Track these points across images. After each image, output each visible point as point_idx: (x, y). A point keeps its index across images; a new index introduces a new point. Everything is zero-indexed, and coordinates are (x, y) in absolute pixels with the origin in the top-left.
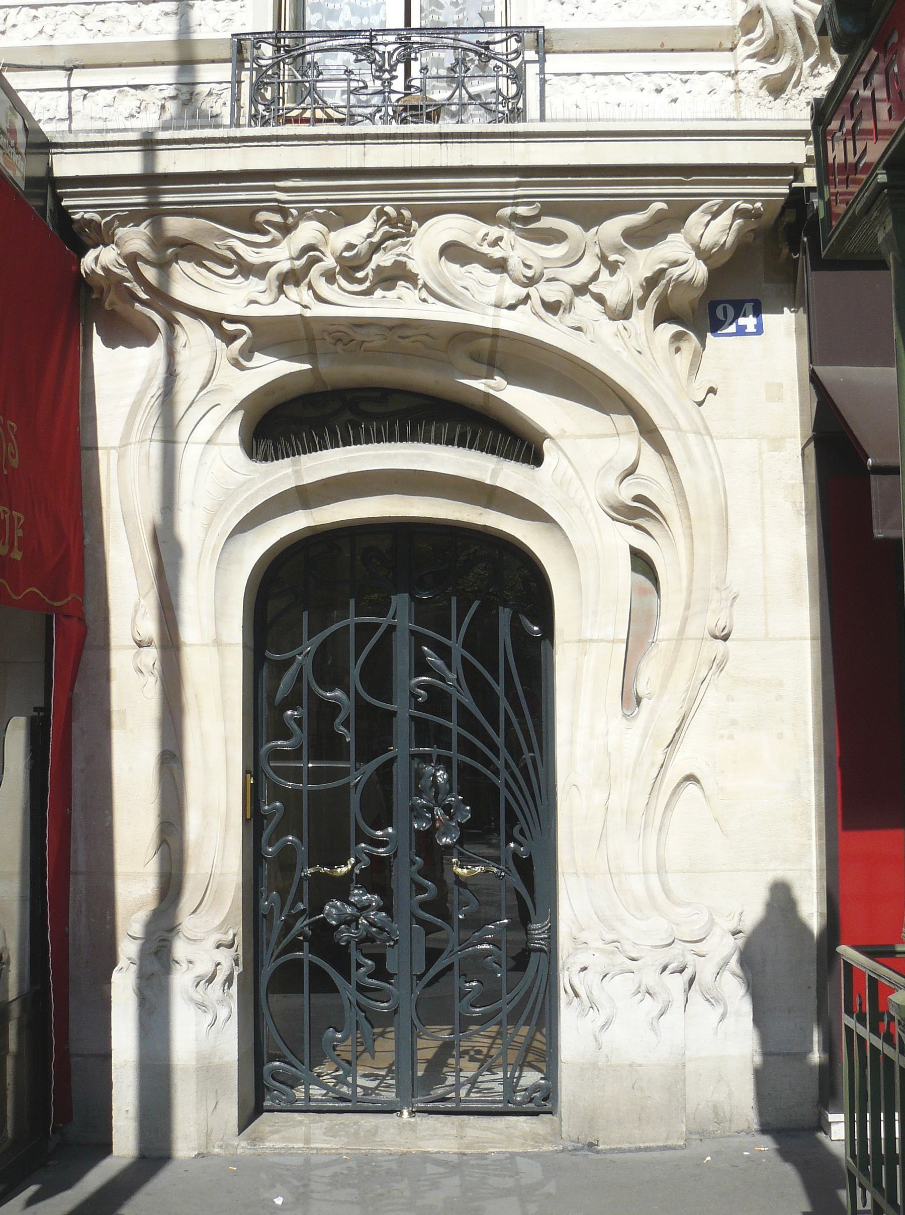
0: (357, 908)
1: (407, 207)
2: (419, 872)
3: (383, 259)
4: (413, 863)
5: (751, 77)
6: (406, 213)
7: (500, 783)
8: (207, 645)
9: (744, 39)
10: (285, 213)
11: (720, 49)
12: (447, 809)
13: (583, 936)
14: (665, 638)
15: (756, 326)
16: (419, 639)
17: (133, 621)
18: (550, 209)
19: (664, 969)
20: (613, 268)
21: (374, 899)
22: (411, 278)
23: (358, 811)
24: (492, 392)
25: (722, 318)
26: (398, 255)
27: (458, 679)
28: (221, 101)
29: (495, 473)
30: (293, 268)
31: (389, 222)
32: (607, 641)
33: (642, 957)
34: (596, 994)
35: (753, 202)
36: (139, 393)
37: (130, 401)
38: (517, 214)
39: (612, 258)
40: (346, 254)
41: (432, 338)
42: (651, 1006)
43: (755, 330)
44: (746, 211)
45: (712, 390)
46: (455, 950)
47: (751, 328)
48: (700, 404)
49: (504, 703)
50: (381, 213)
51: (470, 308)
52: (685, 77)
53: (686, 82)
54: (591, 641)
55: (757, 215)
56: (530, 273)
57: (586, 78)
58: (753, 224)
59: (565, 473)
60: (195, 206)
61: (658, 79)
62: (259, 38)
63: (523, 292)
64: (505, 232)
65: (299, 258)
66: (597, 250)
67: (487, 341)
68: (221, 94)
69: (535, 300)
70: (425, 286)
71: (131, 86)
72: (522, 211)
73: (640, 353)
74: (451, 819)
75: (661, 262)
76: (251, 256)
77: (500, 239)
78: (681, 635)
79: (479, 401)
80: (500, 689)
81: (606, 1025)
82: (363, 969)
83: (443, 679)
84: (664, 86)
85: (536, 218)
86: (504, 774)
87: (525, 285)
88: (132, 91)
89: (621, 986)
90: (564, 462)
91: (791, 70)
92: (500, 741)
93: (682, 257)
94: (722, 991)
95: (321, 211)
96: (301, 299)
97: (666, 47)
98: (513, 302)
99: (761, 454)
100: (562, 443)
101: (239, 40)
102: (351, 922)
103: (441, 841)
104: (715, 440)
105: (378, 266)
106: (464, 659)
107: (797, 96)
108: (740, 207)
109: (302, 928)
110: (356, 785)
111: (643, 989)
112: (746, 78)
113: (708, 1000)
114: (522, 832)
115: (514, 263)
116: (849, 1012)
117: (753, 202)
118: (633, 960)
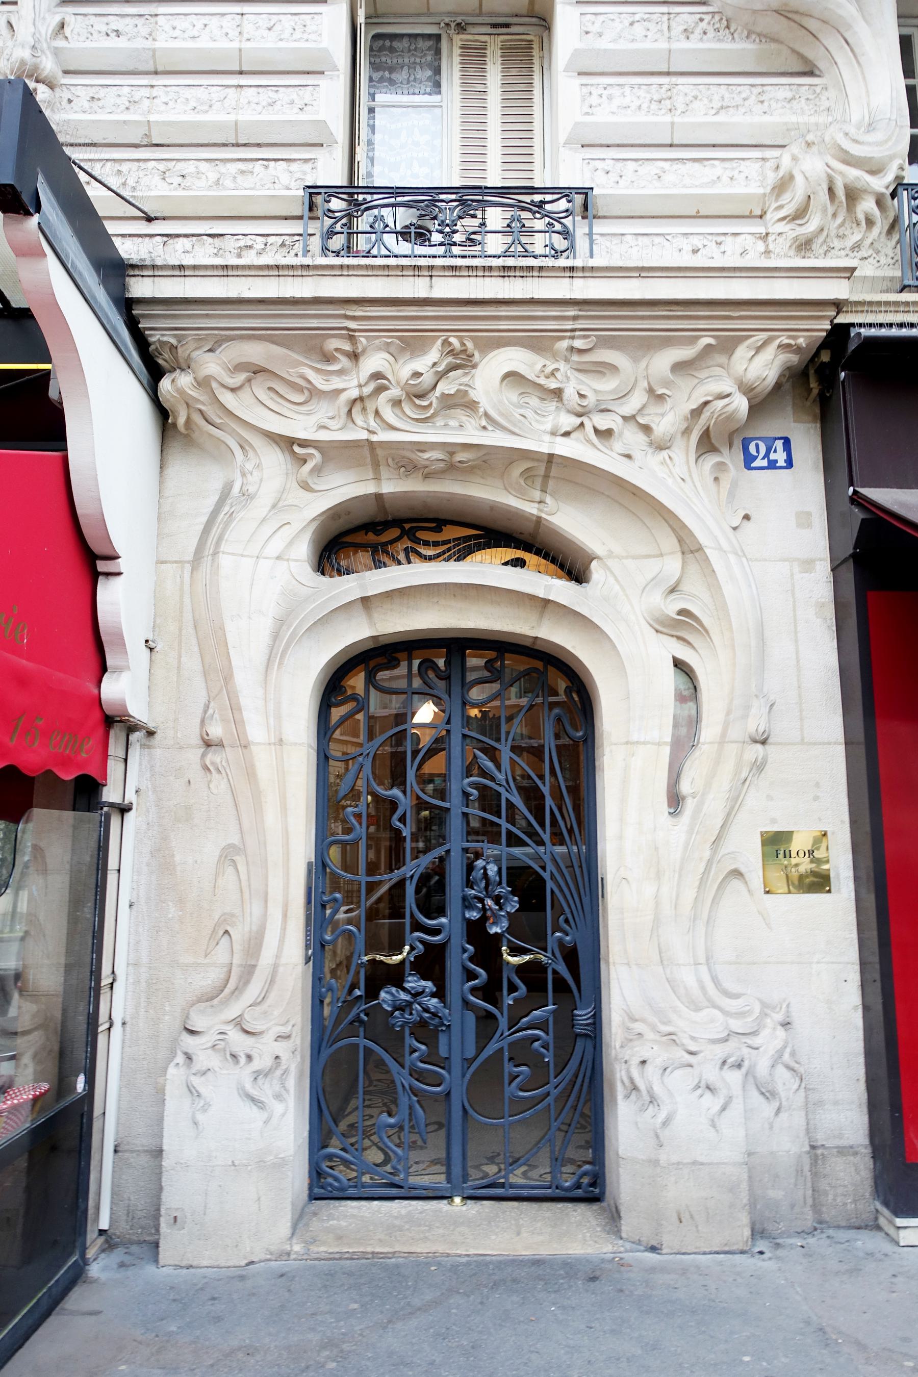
0: (411, 994)
2: (471, 959)
3: (444, 387)
4: (465, 950)
5: (780, 240)
6: (470, 345)
7: (546, 876)
9: (774, 205)
10: (352, 339)
11: (750, 216)
12: (497, 899)
13: (639, 1027)
14: (708, 741)
17: (203, 722)
19: (724, 1062)
21: (429, 985)
22: (471, 406)
23: (413, 901)
24: (544, 516)
25: (755, 453)
26: (460, 385)
28: (293, 253)
31: (452, 352)
32: (653, 744)
33: (701, 1052)
34: (657, 1089)
36: (212, 512)
37: (204, 519)
39: (660, 392)
40: (412, 382)
42: (711, 1103)
44: (789, 345)
45: (747, 517)
47: (781, 463)
49: (549, 802)
50: (446, 342)
51: (527, 435)
52: (720, 239)
53: (720, 244)
54: (637, 742)
55: (798, 350)
57: (629, 238)
62: (332, 191)
63: (578, 421)
64: (562, 365)
66: (646, 385)
70: (486, 414)
71: (209, 235)
72: (579, 344)
73: (683, 480)
74: (501, 909)
75: (706, 395)
76: (318, 382)
77: (557, 370)
78: (723, 740)
79: (529, 527)
80: (546, 790)
81: (665, 1123)
82: (416, 1054)
83: (493, 779)
84: (701, 246)
87: (580, 415)
88: (210, 240)
89: (680, 1080)
90: (611, 580)
93: (728, 390)
96: (369, 425)
97: (701, 214)
98: (568, 429)
99: (792, 575)
100: (610, 562)
101: (311, 194)
102: (402, 1007)
105: (443, 394)
109: (358, 1014)
110: (412, 877)
111: (703, 1084)
113: (763, 1093)
114: (567, 921)
115: (570, 393)
116: (698, 1009)
118: (691, 1053)
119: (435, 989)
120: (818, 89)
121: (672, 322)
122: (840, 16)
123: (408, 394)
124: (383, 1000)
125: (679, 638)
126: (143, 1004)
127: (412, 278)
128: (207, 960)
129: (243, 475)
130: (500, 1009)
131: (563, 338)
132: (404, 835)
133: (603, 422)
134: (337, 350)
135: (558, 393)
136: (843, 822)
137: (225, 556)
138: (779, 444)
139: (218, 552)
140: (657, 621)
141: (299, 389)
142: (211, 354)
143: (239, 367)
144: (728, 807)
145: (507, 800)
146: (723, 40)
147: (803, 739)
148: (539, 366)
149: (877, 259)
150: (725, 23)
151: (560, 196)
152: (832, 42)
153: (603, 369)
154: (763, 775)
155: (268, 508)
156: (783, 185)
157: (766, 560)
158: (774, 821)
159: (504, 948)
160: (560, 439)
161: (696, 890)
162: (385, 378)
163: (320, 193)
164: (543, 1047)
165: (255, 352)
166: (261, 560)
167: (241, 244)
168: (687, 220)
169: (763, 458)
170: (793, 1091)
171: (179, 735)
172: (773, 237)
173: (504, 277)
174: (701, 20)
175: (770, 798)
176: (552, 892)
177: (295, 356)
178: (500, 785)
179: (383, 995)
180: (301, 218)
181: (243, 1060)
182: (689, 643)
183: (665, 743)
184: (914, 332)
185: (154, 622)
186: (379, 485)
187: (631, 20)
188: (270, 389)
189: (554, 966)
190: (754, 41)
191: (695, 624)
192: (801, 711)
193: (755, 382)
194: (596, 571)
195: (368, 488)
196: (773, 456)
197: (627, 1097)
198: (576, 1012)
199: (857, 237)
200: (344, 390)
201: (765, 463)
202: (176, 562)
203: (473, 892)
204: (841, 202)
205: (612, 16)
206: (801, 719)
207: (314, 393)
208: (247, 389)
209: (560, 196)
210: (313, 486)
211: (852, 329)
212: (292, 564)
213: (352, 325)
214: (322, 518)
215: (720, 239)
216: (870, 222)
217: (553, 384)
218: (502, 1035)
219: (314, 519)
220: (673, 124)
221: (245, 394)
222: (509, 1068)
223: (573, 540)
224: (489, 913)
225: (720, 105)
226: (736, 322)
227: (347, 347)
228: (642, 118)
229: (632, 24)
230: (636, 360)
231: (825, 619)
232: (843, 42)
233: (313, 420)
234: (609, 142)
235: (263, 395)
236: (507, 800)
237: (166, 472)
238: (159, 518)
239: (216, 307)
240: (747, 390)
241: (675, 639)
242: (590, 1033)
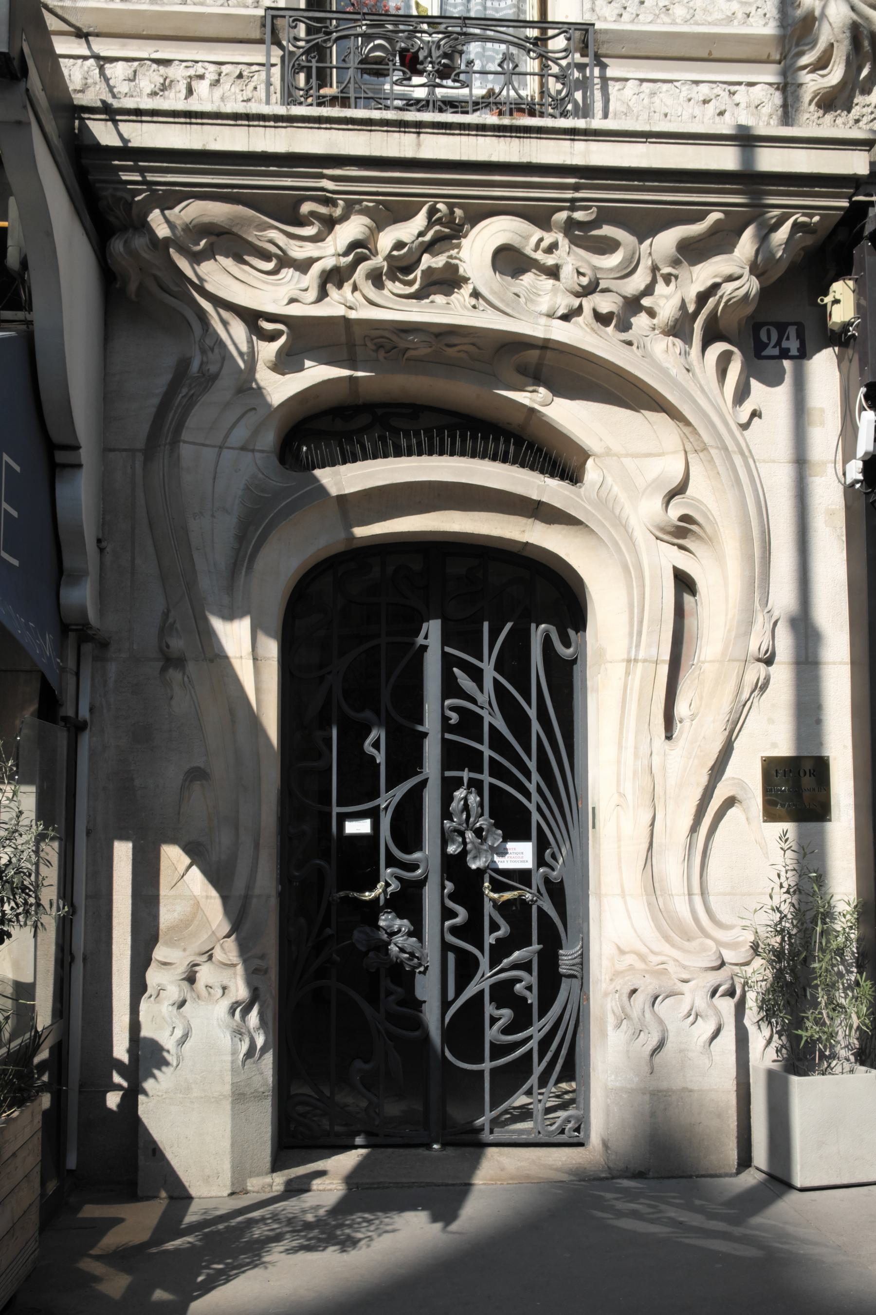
1: (460, 206)
3: (438, 261)
7: (532, 807)
12: (478, 832)
14: (708, 659)
15: (799, 350)
16: (448, 662)
18: (606, 216)
19: (714, 993)
20: (667, 279)
21: (404, 924)
28: (251, 85)
30: (338, 265)
32: (650, 662)
35: (811, 216)
37: (155, 401)
38: (573, 218)
40: (395, 253)
41: (479, 348)
43: (798, 354)
46: (486, 976)
48: (745, 426)
49: (536, 726)
51: (522, 317)
52: (733, 88)
53: (734, 94)
56: (585, 281)
58: (810, 240)
59: (610, 491)
60: (235, 190)
61: (704, 89)
63: (576, 302)
65: (346, 254)
67: (536, 353)
68: (252, 77)
72: (579, 215)
75: (715, 276)
79: (518, 419)
80: (532, 713)
82: (392, 997)
83: (474, 701)
84: (713, 97)
85: (595, 224)
86: (535, 796)
88: (154, 66)
92: (532, 765)
95: (371, 204)
101: (274, 17)
104: (757, 464)
106: (495, 680)
108: (799, 220)
110: (386, 808)
114: (554, 856)
117: (811, 216)
119: (412, 928)
129: (203, 352)
130: (482, 951)
132: (378, 761)
136: (845, 747)
137: (186, 445)
138: (792, 331)
139: (179, 441)
140: (662, 530)
144: (728, 730)
145: (491, 725)
148: (534, 240)
151: (557, 31)
153: (608, 246)
157: (774, 461)
159: (486, 884)
163: (284, 17)
166: (225, 451)
167: (191, 72)
168: (699, 63)
169: (774, 347)
171: (135, 647)
176: (538, 824)
178: (482, 708)
180: (261, 41)
183: (663, 661)
185: (103, 519)
189: (540, 903)
194: (592, 472)
196: (785, 344)
197: (618, 1026)
198: (561, 951)
200: (318, 259)
201: (776, 352)
207: (285, 261)
209: (557, 31)
211: (870, 209)
212: (258, 455)
217: (550, 260)
218: (483, 976)
222: (489, 1009)
223: (569, 434)
224: (469, 847)
231: (835, 528)
236: (491, 725)
238: (105, 399)
241: (676, 547)
242: (575, 973)
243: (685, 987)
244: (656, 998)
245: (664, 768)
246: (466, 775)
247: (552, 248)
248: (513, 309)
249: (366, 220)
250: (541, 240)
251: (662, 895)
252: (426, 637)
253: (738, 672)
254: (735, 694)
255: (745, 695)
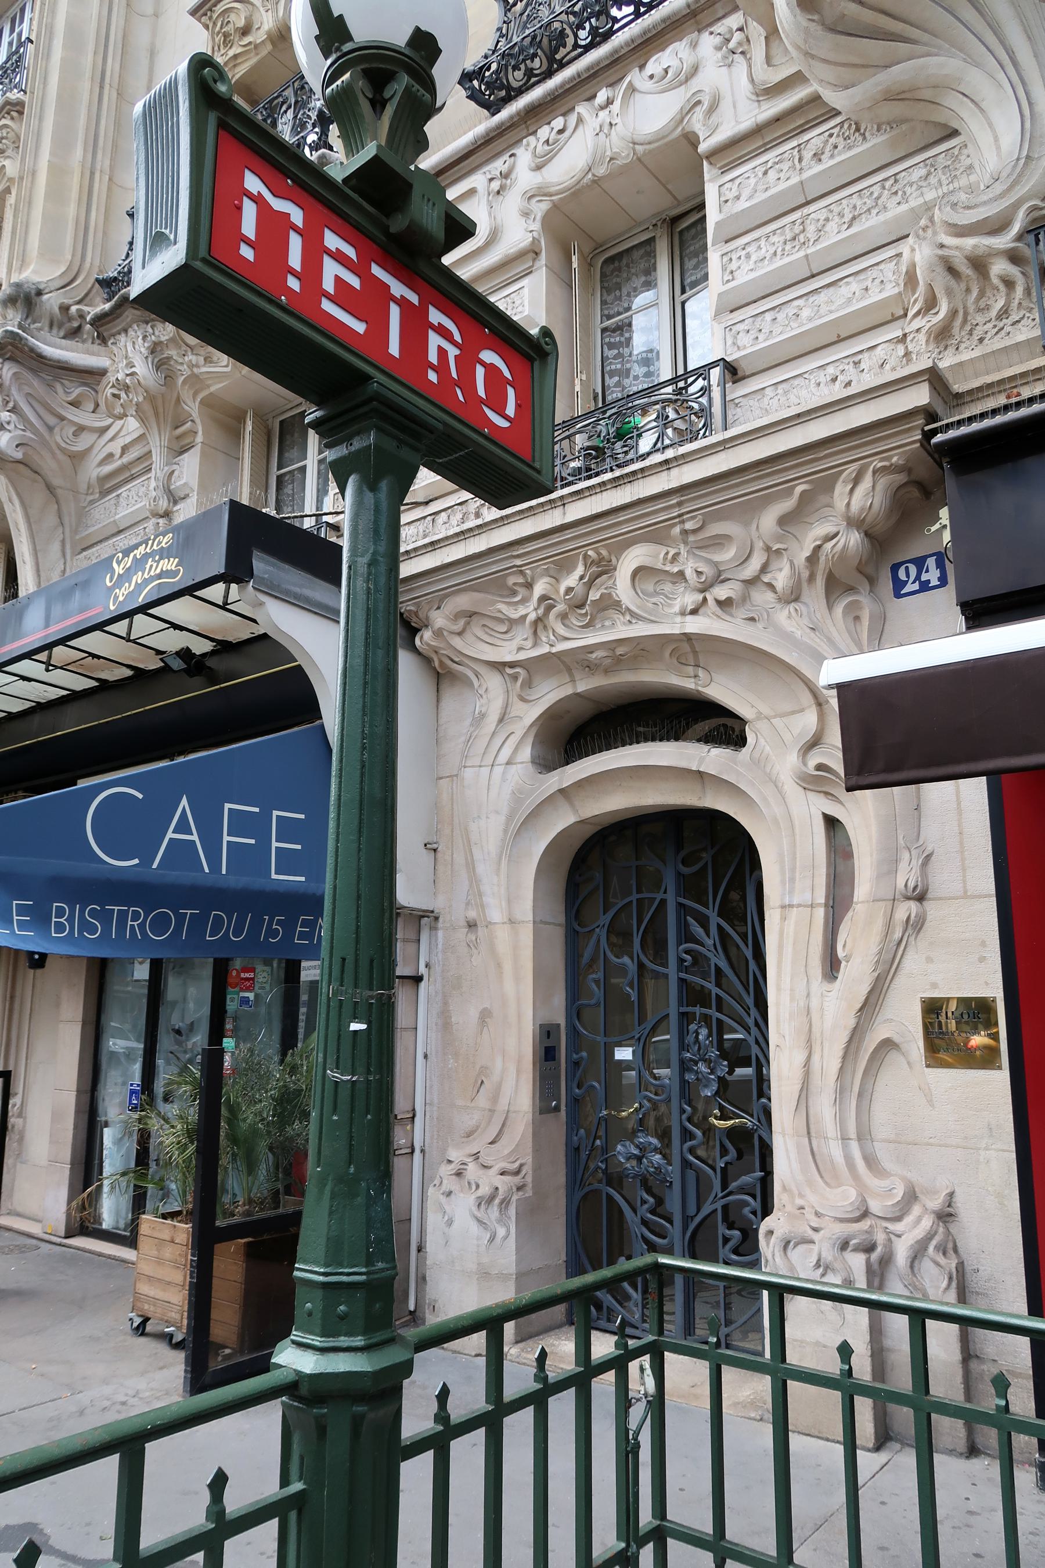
3: (594, 595)
6: (604, 552)
8: (505, 923)
11: (894, 319)
14: (860, 900)
15: (939, 579)
22: (617, 605)
24: (700, 689)
27: (715, 945)
29: (702, 760)
32: (805, 906)
40: (567, 597)
44: (884, 468)
47: (934, 582)
50: (586, 556)
51: (658, 620)
52: (856, 359)
53: (859, 362)
61: (831, 370)
63: (700, 597)
69: (711, 601)
70: (628, 609)
72: (689, 526)
75: (815, 541)
77: (678, 554)
82: (646, 1206)
84: (838, 374)
88: (460, 507)
91: (953, 313)
93: (834, 530)
94: (922, 1278)
103: (703, 1092)
106: (718, 925)
107: (967, 337)
112: (914, 337)
115: (689, 573)
120: (956, 151)
121: (765, 480)
122: (946, 75)
123: (570, 607)
124: (619, 1152)
125: (826, 793)
126: (435, 1137)
127: (551, 511)
128: (473, 1105)
131: (674, 525)
133: (722, 592)
134: (515, 584)
135: (681, 574)
138: (931, 562)
141: (500, 621)
142: (438, 611)
143: (457, 616)
146: (853, 146)
147: (965, 892)
149: (1032, 317)
150: (854, 126)
152: (952, 101)
154: (921, 934)
155: (495, 724)
156: (911, 280)
158: (934, 986)
160: (689, 618)
161: (840, 1060)
162: (551, 599)
164: (752, 1213)
165: (463, 601)
169: (914, 582)
170: (941, 1289)
172: (912, 336)
173: (616, 487)
174: (831, 135)
175: (929, 960)
176: (757, 1056)
177: (490, 597)
179: (619, 1147)
181: (474, 1187)
182: (832, 795)
184: (1037, 408)
186: (575, 687)
187: (764, 169)
188: (484, 625)
190: (886, 130)
191: (834, 778)
192: (963, 860)
193: (860, 517)
195: (567, 691)
196: (924, 577)
198: (144, 1216)
199: (1001, 303)
202: (448, 777)
203: (688, 1055)
204: (968, 276)
205: (746, 175)
206: (964, 870)
208: (468, 631)
210: (527, 698)
212: (519, 766)
213: (518, 562)
214: (539, 723)
215: (856, 359)
216: (1009, 284)
219: (531, 725)
220: (807, 256)
221: (468, 636)
225: (851, 216)
226: (824, 461)
227: (521, 580)
228: (779, 263)
229: (765, 173)
230: (747, 524)
232: (961, 96)
233: (514, 644)
234: (754, 298)
235: (480, 633)
237: (441, 704)
239: (436, 574)
240: (853, 523)
241: (822, 794)
243: (816, 1237)
244: (789, 1242)
245: (822, 1009)
246: (698, 1010)
247: (675, 558)
248: (655, 616)
249: (547, 579)
250: (667, 553)
251: (816, 1138)
252: (665, 892)
253: (885, 912)
254: (884, 933)
255: (897, 935)
